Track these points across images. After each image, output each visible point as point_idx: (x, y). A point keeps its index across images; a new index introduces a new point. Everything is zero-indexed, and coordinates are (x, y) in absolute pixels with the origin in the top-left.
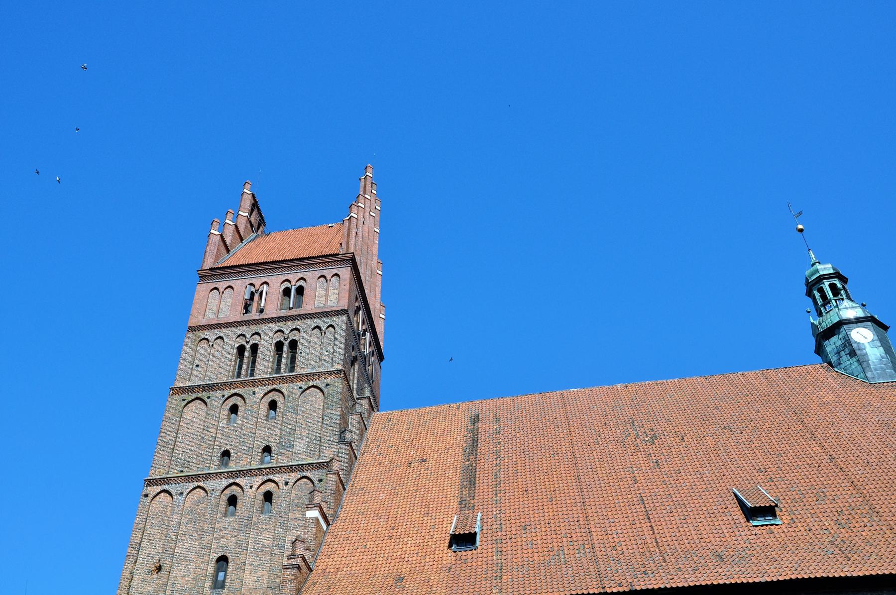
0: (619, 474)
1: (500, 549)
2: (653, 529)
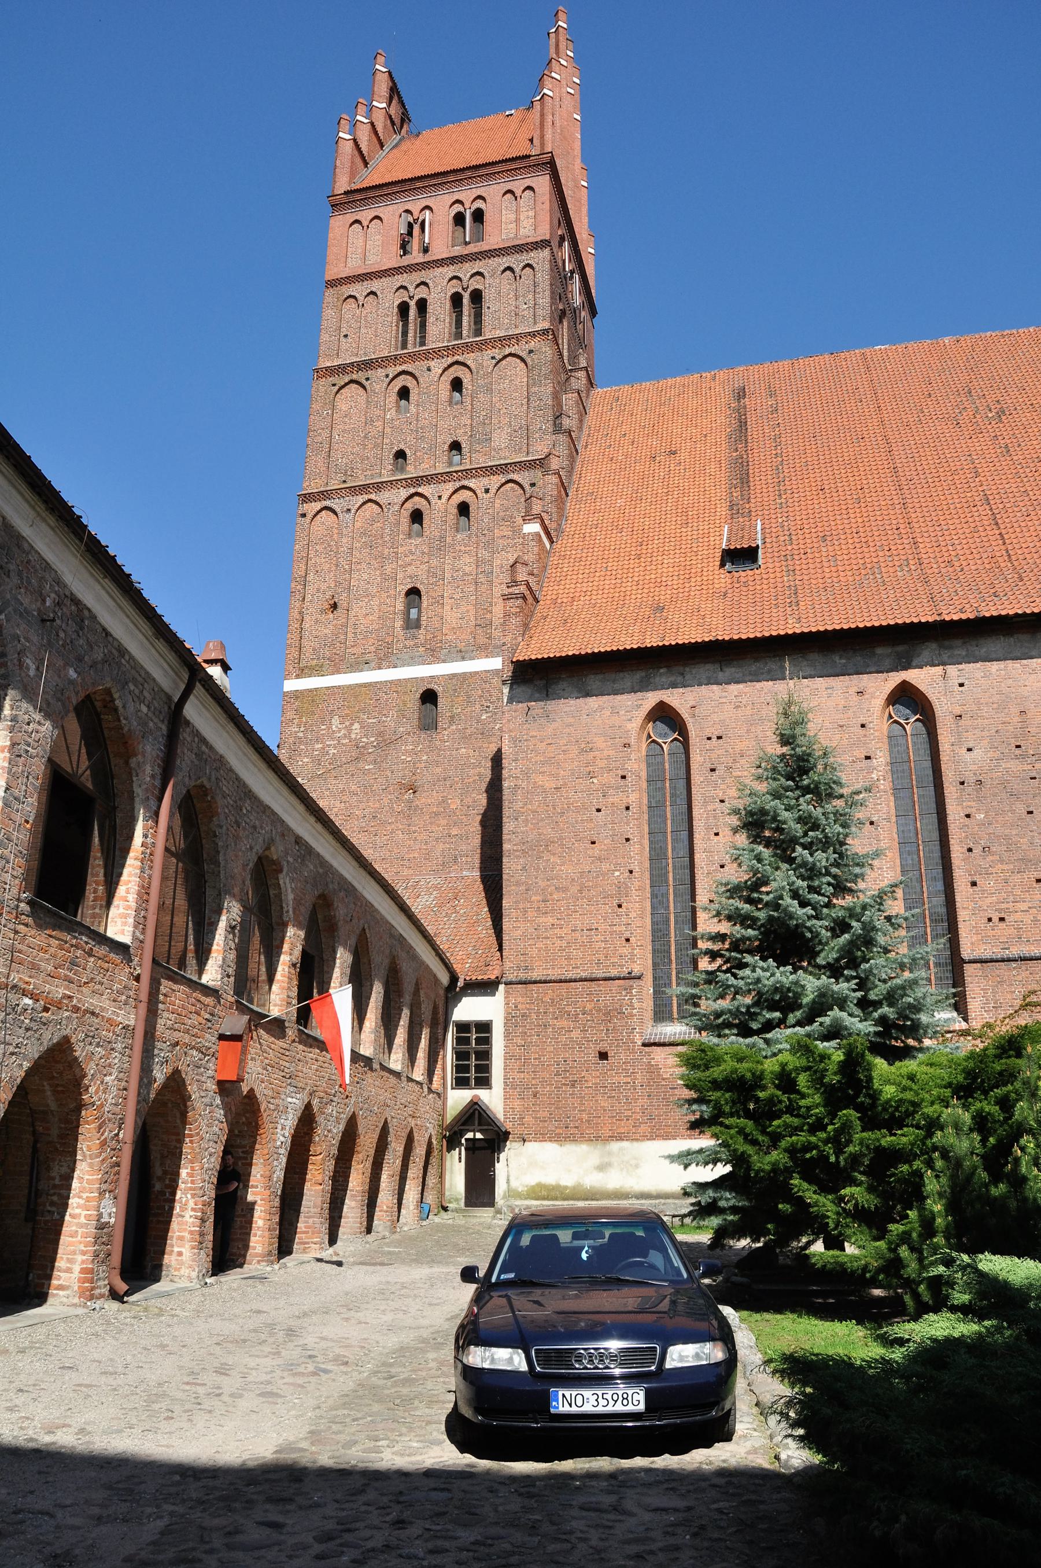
0: (952, 464)
1: (791, 568)
2: (1003, 538)
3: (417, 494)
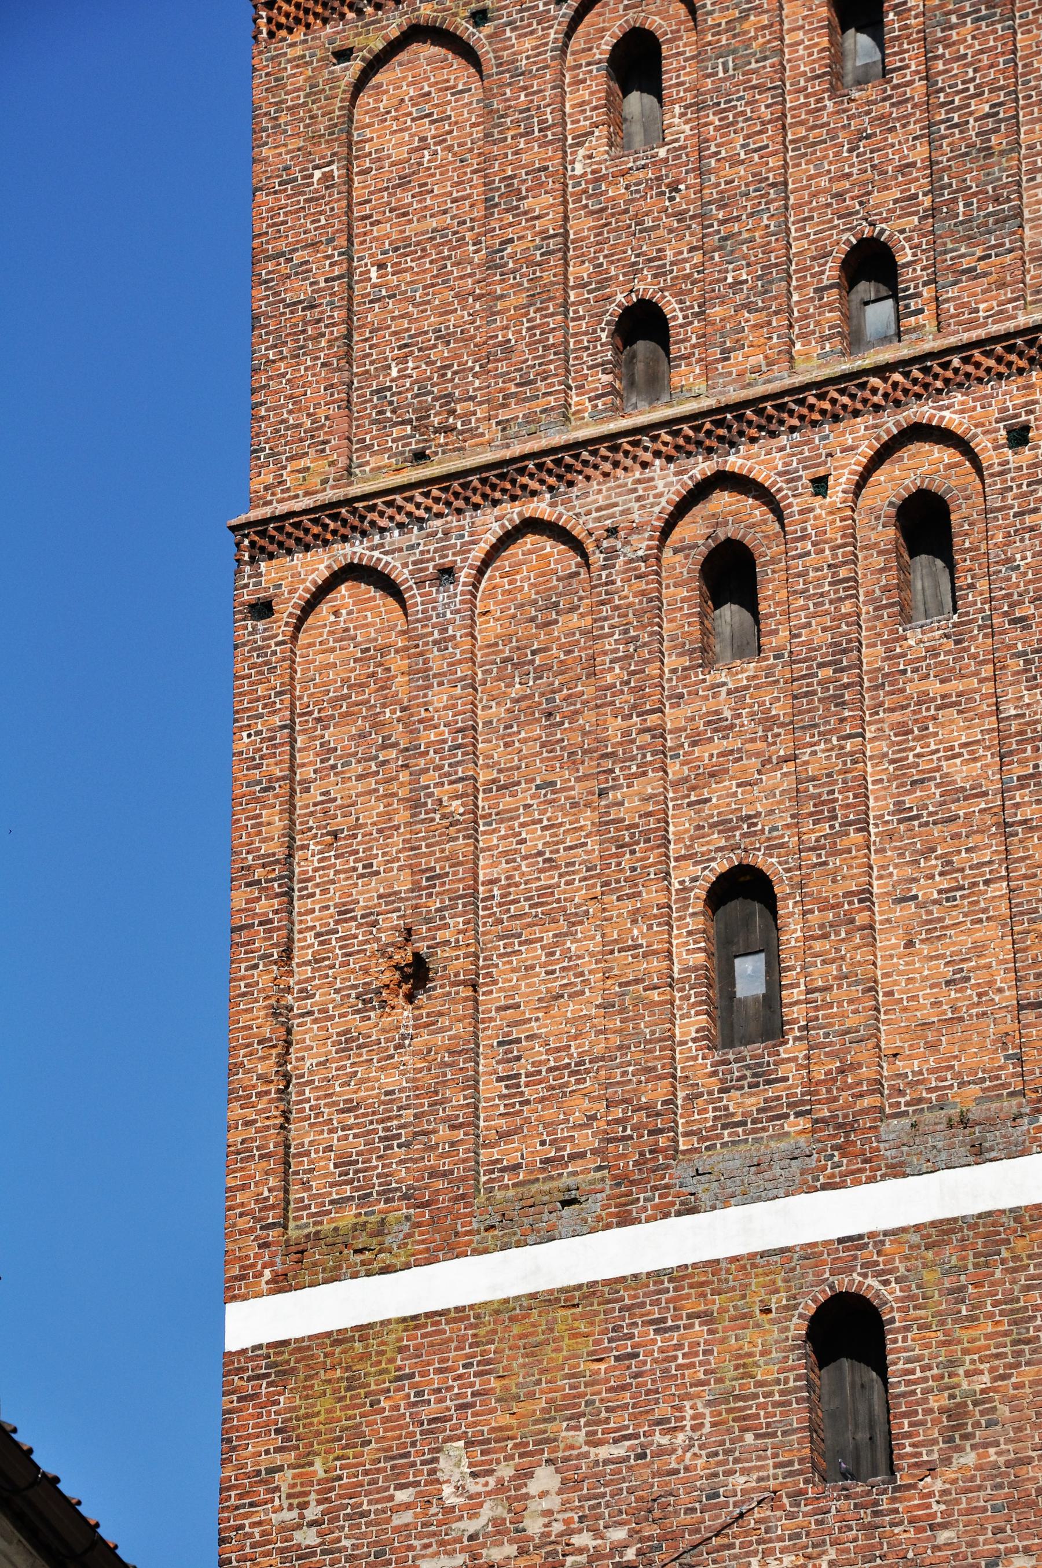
3: (724, 480)
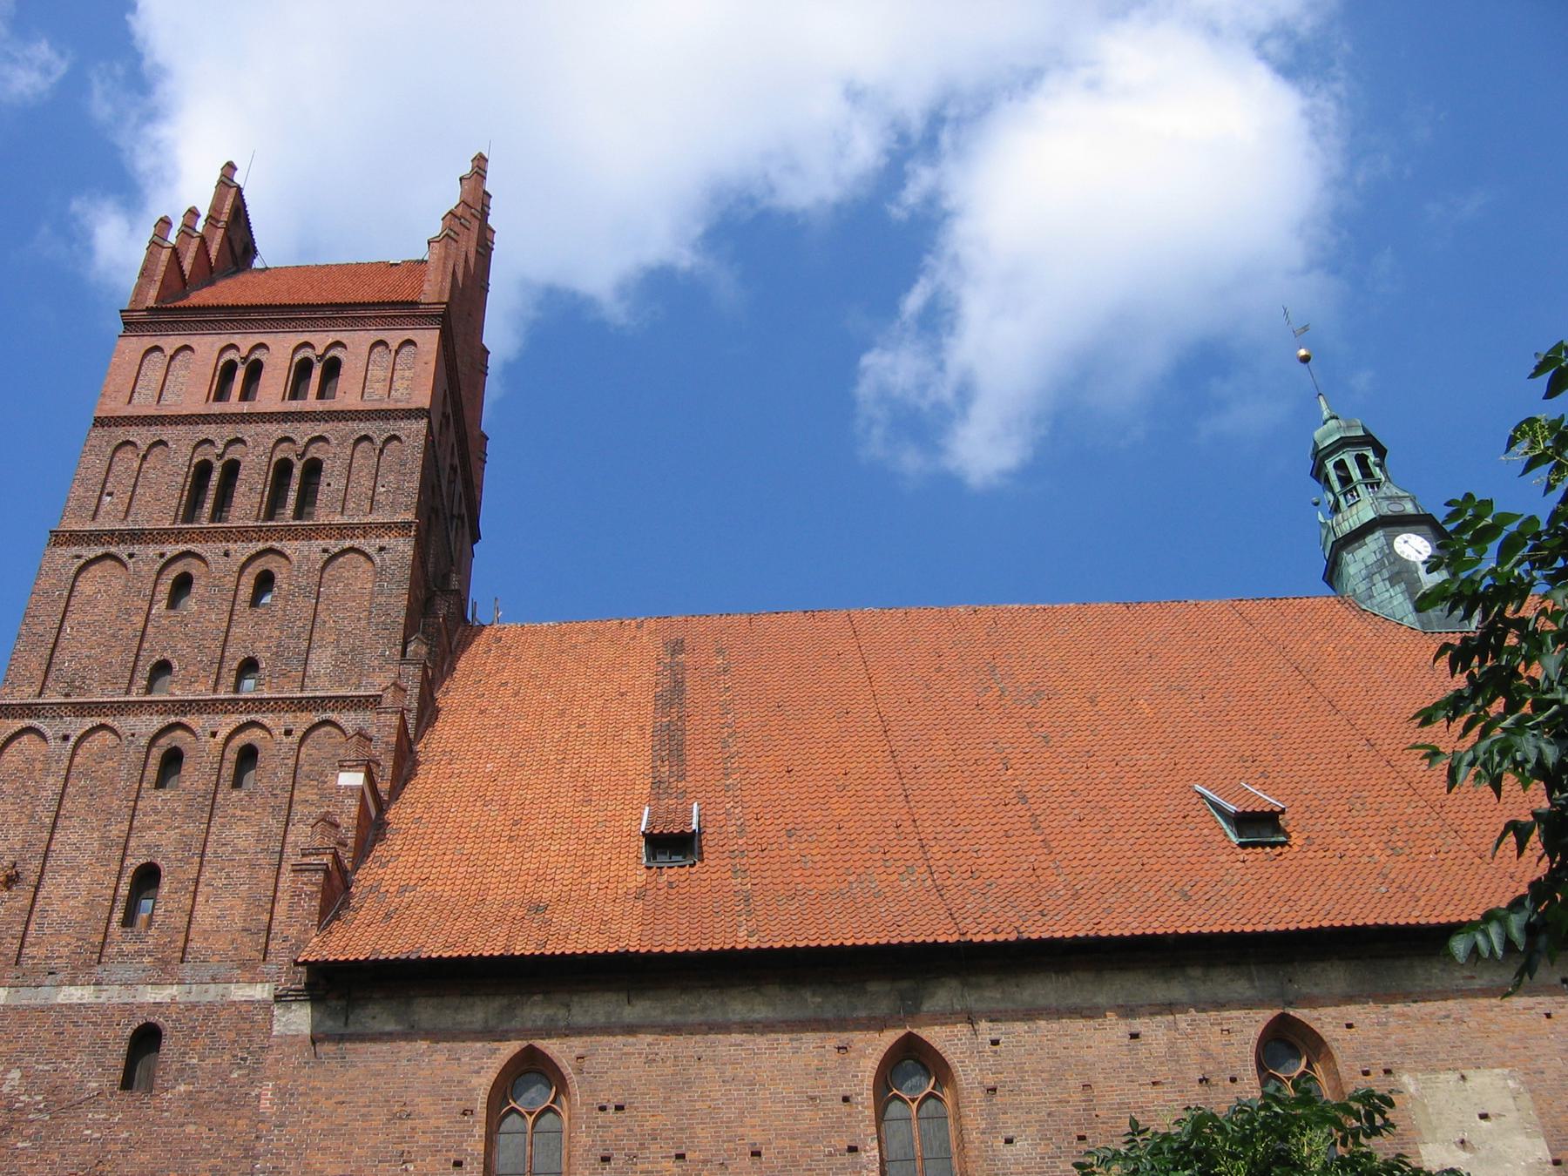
3: (179, 725)
